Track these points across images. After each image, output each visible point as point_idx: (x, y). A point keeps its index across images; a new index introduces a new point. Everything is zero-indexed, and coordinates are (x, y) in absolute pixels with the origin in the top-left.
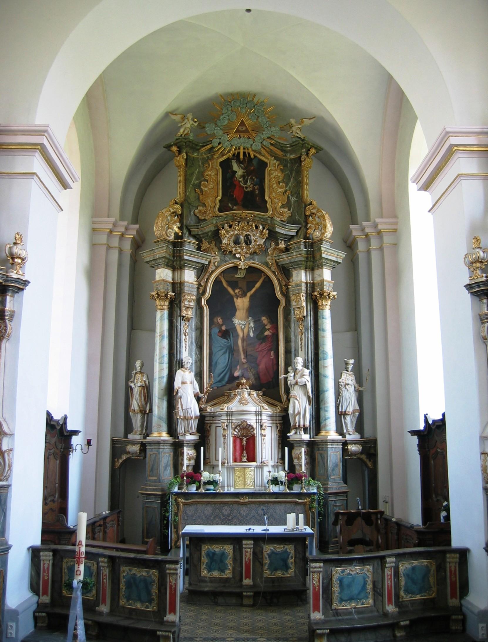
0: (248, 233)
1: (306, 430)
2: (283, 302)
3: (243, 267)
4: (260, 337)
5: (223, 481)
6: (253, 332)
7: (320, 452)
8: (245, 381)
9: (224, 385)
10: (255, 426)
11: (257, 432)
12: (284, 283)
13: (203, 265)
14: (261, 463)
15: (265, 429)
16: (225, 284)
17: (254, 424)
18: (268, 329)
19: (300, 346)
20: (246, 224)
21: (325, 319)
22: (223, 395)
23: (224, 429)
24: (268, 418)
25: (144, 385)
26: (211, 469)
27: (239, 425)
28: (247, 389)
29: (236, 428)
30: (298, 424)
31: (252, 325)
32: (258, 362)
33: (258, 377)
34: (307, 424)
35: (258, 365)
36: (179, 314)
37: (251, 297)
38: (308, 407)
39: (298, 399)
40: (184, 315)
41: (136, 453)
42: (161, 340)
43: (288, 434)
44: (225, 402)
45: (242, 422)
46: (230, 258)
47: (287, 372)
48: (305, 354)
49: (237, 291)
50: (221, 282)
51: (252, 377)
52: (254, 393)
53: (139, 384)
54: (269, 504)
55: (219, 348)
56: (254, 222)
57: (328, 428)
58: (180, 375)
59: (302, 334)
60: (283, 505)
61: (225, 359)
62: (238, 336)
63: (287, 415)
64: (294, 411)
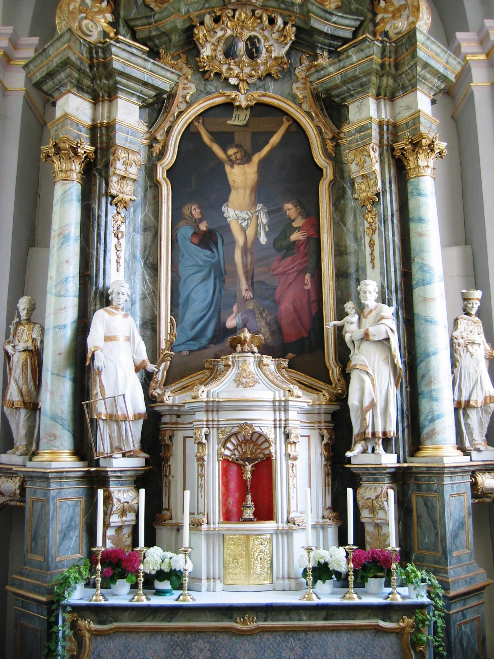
0: (253, 33)
1: (387, 442)
2: (328, 173)
3: (244, 104)
4: (281, 244)
5: (197, 567)
6: (267, 234)
7: (423, 494)
8: (248, 335)
9: (205, 347)
10: (271, 437)
11: (278, 450)
12: (330, 136)
13: (160, 92)
14: (288, 522)
15: (295, 443)
16: (206, 138)
17: (269, 433)
18: (298, 229)
19: (368, 259)
20: (250, 14)
21: (425, 195)
22: (202, 368)
23: (200, 444)
24: (303, 418)
25: (31, 348)
26: (174, 533)
27: (236, 434)
28: (253, 353)
29: (228, 440)
30: (370, 430)
31: (264, 219)
32: (277, 296)
33: (277, 329)
34: (392, 429)
35: (277, 303)
36: (103, 191)
37: (261, 163)
38: (394, 392)
39: (370, 372)
40: (114, 192)
41: (15, 494)
42: (62, 244)
43: (348, 454)
44: (205, 382)
45: (240, 426)
46: (216, 88)
47: (341, 314)
48: (382, 274)
49: (231, 151)
50: (198, 134)
51: (265, 329)
52: (268, 360)
53: (21, 346)
54: (310, 634)
55: (195, 269)
56: (267, 11)
57: (439, 438)
58: (100, 319)
59: (374, 232)
60: (345, 637)
61: (207, 292)
62: (233, 242)
63: (345, 409)
64: (361, 401)
